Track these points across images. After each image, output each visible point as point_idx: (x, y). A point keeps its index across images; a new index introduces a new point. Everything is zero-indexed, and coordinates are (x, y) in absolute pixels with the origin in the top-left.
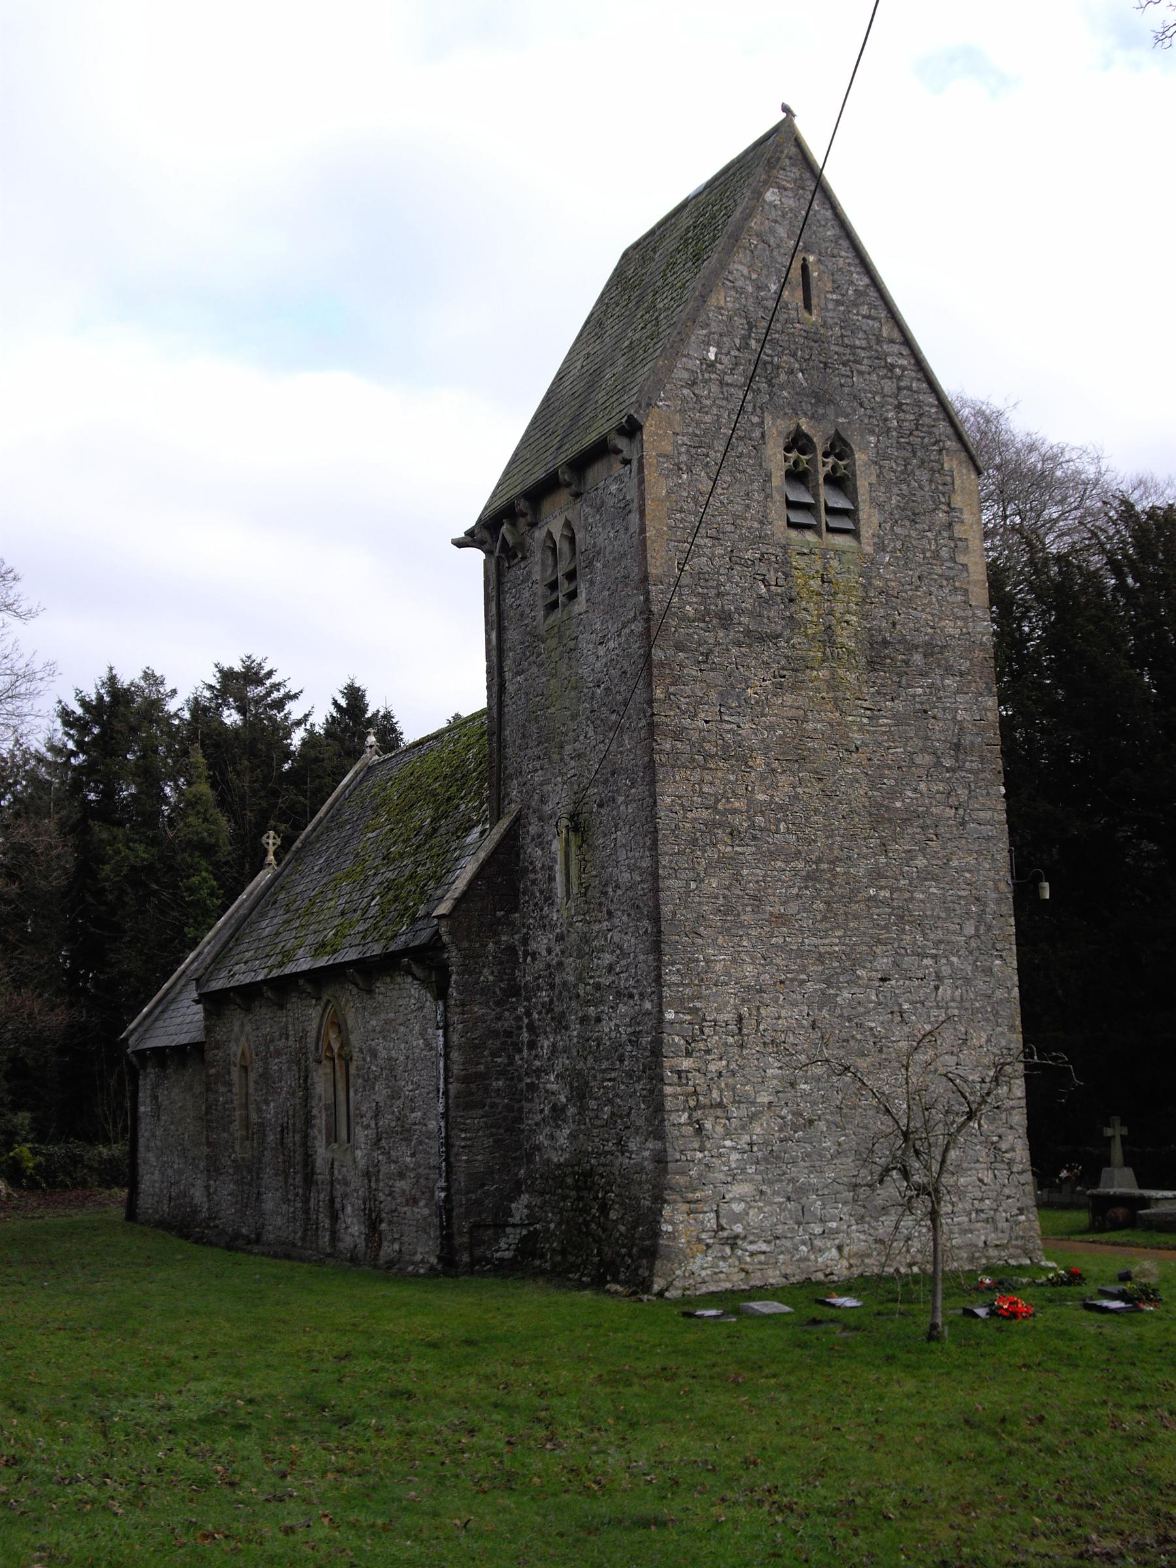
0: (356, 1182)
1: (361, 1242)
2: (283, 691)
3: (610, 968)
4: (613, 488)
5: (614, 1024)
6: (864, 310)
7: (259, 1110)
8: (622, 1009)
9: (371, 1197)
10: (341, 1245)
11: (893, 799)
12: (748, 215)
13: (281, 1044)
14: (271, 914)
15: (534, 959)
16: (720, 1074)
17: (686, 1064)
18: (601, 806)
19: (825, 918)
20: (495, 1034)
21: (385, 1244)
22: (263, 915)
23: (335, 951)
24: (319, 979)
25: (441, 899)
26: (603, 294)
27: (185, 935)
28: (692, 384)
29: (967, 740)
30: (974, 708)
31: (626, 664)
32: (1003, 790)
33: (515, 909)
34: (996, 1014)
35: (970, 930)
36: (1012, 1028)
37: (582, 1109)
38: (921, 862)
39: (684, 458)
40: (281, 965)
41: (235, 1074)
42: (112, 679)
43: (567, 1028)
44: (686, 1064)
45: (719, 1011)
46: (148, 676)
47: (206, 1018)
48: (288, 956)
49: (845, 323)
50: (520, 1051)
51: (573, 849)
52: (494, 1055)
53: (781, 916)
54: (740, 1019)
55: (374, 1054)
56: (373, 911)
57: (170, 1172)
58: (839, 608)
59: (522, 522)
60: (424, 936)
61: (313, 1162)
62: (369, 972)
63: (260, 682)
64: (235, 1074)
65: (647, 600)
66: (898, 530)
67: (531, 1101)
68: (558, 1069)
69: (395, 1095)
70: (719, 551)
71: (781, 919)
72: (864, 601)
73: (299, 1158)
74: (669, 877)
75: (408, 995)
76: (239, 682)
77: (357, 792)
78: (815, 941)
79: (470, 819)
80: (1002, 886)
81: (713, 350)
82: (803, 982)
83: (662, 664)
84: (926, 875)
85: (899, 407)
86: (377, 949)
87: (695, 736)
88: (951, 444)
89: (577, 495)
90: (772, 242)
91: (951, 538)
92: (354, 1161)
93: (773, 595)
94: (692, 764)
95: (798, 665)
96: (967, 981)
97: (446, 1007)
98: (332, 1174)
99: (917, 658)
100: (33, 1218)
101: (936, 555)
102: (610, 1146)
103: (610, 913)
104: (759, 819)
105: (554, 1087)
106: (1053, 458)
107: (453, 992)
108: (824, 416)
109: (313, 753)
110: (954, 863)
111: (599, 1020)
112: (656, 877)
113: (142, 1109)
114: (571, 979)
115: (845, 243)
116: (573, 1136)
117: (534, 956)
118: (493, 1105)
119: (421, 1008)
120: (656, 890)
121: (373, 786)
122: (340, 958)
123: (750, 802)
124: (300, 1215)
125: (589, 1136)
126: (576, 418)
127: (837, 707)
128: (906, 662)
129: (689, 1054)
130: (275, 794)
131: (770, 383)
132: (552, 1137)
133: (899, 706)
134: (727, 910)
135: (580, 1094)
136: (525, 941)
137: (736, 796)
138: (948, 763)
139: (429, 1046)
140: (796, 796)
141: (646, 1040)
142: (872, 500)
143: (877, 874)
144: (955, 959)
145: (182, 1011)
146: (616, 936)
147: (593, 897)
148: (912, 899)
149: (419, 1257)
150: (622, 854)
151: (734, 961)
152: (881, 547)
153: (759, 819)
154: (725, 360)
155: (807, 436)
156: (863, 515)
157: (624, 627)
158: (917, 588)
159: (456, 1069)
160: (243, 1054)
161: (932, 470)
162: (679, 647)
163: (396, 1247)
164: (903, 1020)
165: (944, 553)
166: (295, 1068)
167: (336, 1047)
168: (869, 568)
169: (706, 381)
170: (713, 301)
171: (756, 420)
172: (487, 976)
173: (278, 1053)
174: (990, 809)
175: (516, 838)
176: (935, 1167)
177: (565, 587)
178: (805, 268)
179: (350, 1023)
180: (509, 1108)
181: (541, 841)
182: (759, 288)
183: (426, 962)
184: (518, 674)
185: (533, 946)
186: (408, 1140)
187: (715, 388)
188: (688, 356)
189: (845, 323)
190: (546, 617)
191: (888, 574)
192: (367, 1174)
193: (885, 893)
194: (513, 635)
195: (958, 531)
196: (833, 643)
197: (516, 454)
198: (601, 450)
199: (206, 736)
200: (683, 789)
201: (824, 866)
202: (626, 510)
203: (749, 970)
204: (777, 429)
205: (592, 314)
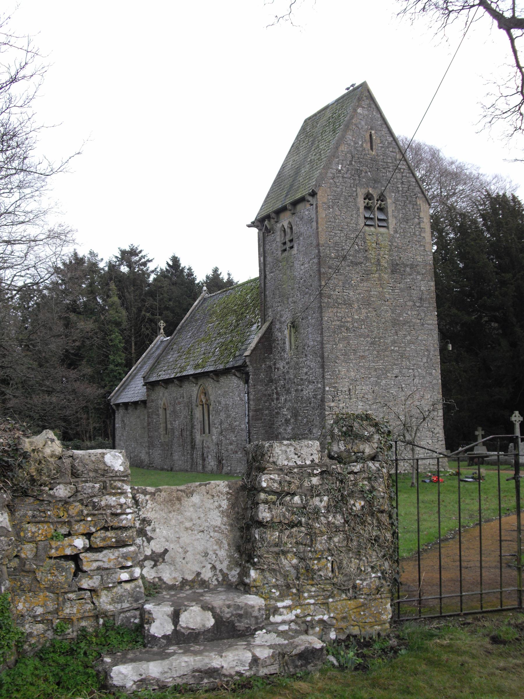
0: (213, 447)
1: (215, 468)
2: (146, 259)
3: (306, 373)
4: (307, 213)
5: (308, 391)
6: (391, 149)
7: (171, 424)
8: (310, 387)
9: (219, 452)
10: (206, 469)
11: (400, 317)
12: (352, 118)
13: (181, 400)
14: (171, 353)
15: (278, 370)
16: (343, 408)
17: (332, 404)
18: (302, 319)
19: (377, 357)
20: (265, 395)
21: (224, 468)
22: (168, 354)
23: (204, 367)
24: (197, 377)
25: (246, 349)
26: (298, 136)
27: (109, 358)
28: (333, 178)
29: (424, 297)
30: (427, 286)
31: (311, 273)
32: (436, 313)
33: (271, 353)
34: (433, 388)
35: (425, 360)
36: (438, 393)
37: (296, 420)
38: (409, 338)
39: (331, 204)
40: (181, 372)
41: (161, 411)
42: (76, 254)
43: (290, 393)
44: (332, 404)
45: (343, 387)
46: (91, 253)
47: (147, 391)
48: (183, 369)
49: (384, 154)
50: (273, 401)
51: (293, 333)
52: (265, 402)
53: (363, 356)
54: (350, 390)
55: (220, 403)
56: (217, 353)
57: (130, 448)
58: (382, 253)
59: (272, 220)
60: (240, 363)
61: (195, 441)
62: (217, 374)
63: (137, 255)
64: (161, 411)
65: (319, 252)
66: (402, 226)
67: (277, 418)
68: (287, 407)
69: (228, 416)
70: (342, 235)
71: (363, 357)
72: (390, 250)
73: (189, 440)
74: (327, 344)
75: (234, 382)
76: (128, 255)
77: (201, 308)
78: (374, 364)
79: (252, 322)
80: (436, 346)
81: (340, 166)
82: (370, 378)
83: (324, 273)
84: (410, 342)
85: (402, 183)
86: (221, 367)
87: (335, 297)
88: (420, 195)
89: (293, 214)
90: (360, 127)
91: (420, 228)
92: (212, 440)
93: (360, 249)
94: (333, 307)
95: (368, 273)
96: (424, 377)
97: (248, 386)
98: (203, 445)
99: (408, 269)
100: (183, 639)
101: (414, 234)
102: (306, 432)
103: (306, 355)
104: (355, 324)
105: (286, 413)
106: (461, 168)
107: (251, 381)
108: (377, 187)
109: (159, 284)
110: (420, 338)
111: (302, 390)
112: (322, 344)
113: (117, 425)
114: (292, 377)
115: (384, 126)
116: (293, 429)
117: (278, 369)
118: (265, 419)
119: (239, 387)
120: (322, 348)
121: (208, 306)
122: (206, 369)
123: (353, 318)
124: (190, 460)
125: (299, 429)
126: (292, 186)
127: (381, 286)
128: (404, 271)
129: (333, 401)
130: (143, 301)
131: (359, 177)
132: (285, 429)
133: (402, 286)
134: (345, 354)
135: (295, 415)
136: (275, 364)
137: (348, 317)
138: (418, 304)
139: (241, 400)
140: (368, 317)
141: (319, 397)
142: (393, 215)
143: (394, 342)
144: (420, 370)
145: (132, 389)
146: (308, 363)
147: (300, 350)
148: (405, 350)
149: (238, 471)
150: (310, 336)
151: (348, 371)
152: (396, 232)
153: (355, 324)
154: (344, 169)
155: (371, 194)
156: (390, 221)
157: (311, 260)
158: (408, 245)
159: (252, 407)
160: (164, 404)
161: (413, 205)
162: (330, 268)
163: (229, 468)
164: (402, 391)
165: (417, 233)
166: (187, 408)
167: (204, 401)
168: (392, 239)
169: (338, 177)
170: (340, 149)
171: (354, 189)
172: (262, 376)
173: (179, 403)
174: (432, 320)
175: (271, 329)
176: (413, 435)
177: (289, 245)
178: (371, 135)
179: (210, 393)
180: (270, 420)
181: (280, 330)
182: (355, 143)
183: (241, 371)
184: (272, 273)
185: (278, 366)
186: (234, 432)
187: (341, 179)
188: (332, 168)
189: (384, 154)
190: (282, 254)
191: (398, 241)
192: (218, 444)
193: (397, 348)
194: (269, 259)
195: (422, 225)
196: (380, 265)
197: (268, 195)
198: (302, 200)
199: (116, 277)
200: (331, 315)
201: (377, 340)
202: (311, 221)
203: (352, 374)
204: (361, 192)
205: (294, 143)
